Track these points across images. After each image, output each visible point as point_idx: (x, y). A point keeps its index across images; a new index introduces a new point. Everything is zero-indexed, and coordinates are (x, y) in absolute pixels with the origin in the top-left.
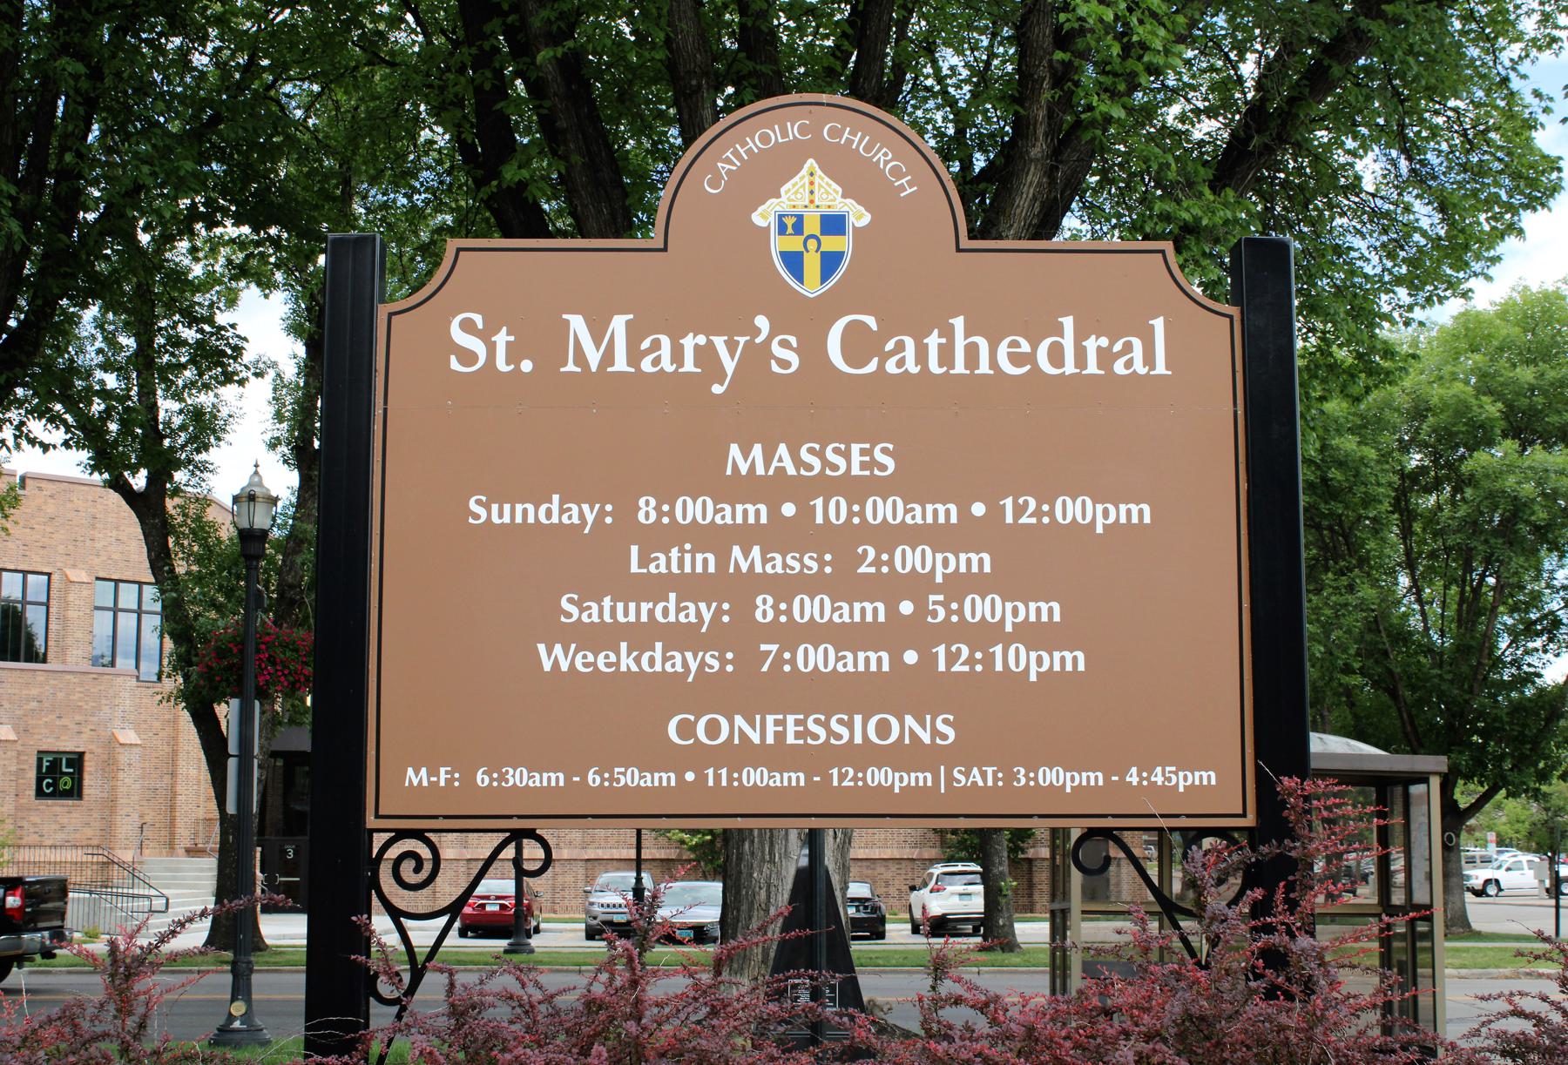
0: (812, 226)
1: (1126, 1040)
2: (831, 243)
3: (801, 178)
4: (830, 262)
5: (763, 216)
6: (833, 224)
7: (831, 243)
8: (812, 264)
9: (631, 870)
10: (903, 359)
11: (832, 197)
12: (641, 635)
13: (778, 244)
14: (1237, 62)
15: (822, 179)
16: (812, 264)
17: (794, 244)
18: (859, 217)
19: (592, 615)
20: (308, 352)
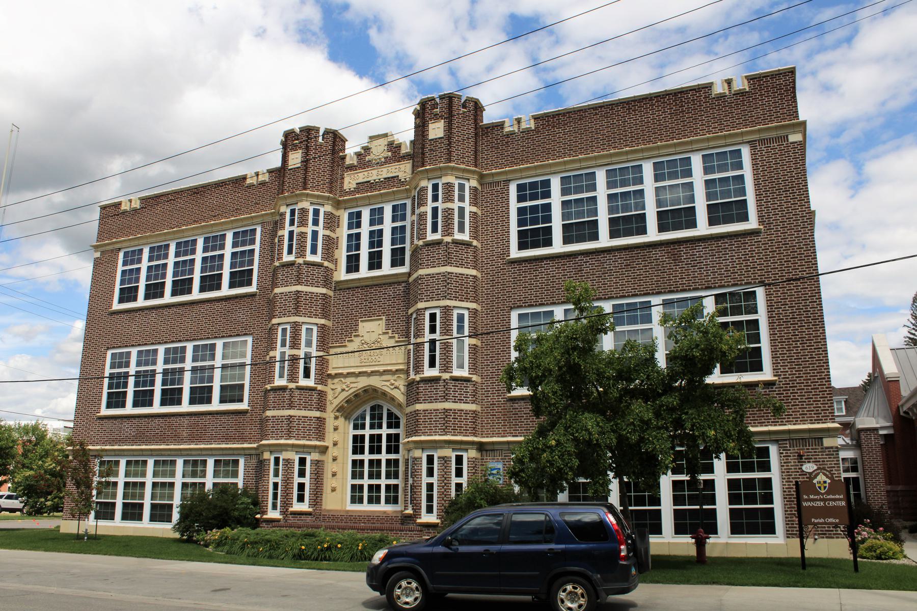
0: (822, 483)
1: (540, 365)
2: (825, 485)
3: (820, 476)
4: (825, 487)
5: (815, 481)
6: (825, 482)
7: (825, 485)
8: (822, 488)
9: (810, 558)
10: (828, 497)
11: (824, 478)
12: (742, 134)
13: (817, 485)
14: (700, 544)
15: (823, 476)
16: (822, 488)
17: (820, 485)
18: (828, 481)
19: (816, 521)
20: (367, 38)
